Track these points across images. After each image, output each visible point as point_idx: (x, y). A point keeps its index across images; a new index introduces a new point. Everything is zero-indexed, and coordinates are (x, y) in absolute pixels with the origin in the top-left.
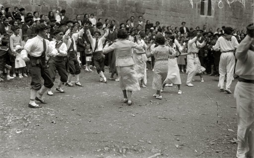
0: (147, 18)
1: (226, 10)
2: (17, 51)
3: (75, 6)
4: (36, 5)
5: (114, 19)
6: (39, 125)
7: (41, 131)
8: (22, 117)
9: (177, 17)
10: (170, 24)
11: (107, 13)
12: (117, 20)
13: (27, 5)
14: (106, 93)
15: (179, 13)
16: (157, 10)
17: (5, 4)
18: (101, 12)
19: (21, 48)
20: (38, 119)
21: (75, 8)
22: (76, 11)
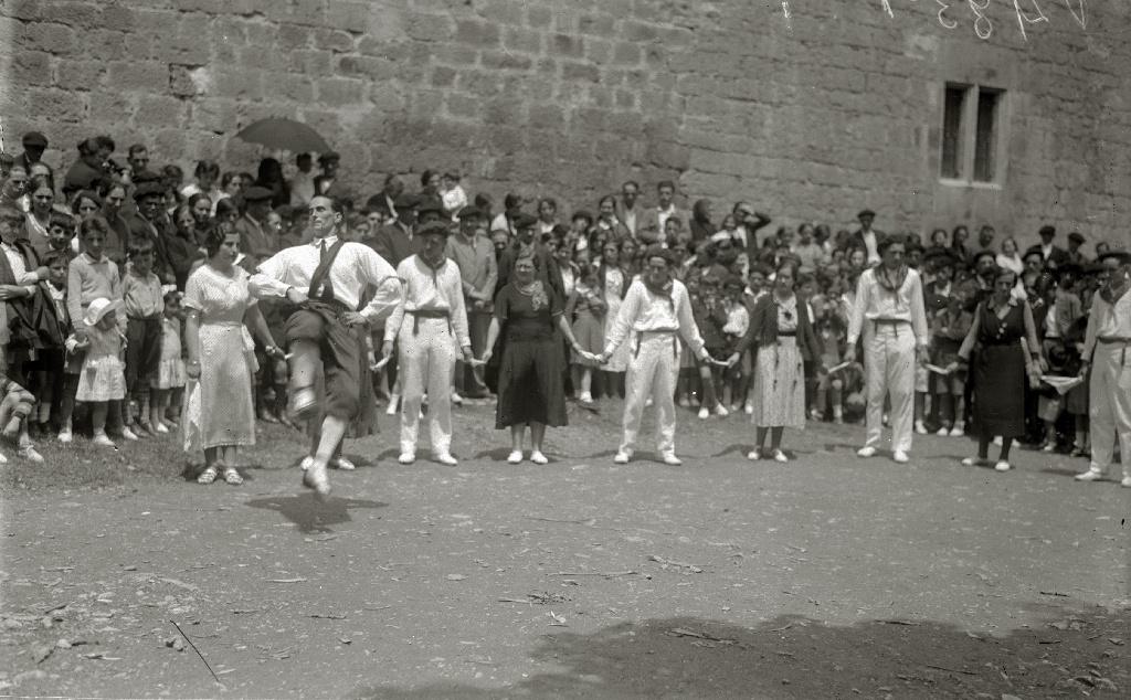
0: (694, 190)
1: (1058, 159)
2: (97, 326)
3: (374, 135)
4: (203, 132)
5: (550, 194)
6: (103, 653)
7: (102, 684)
8: (33, 618)
9: (832, 186)
10: (799, 217)
11: (518, 166)
12: (560, 195)
13: (164, 129)
14: (465, 517)
15: (841, 167)
16: (743, 153)
17: (70, 124)
18: (492, 160)
19: (112, 308)
20: (108, 629)
21: (376, 145)
22: (380, 157)
